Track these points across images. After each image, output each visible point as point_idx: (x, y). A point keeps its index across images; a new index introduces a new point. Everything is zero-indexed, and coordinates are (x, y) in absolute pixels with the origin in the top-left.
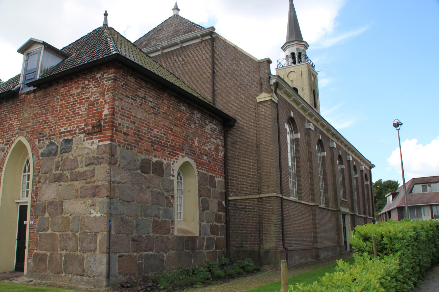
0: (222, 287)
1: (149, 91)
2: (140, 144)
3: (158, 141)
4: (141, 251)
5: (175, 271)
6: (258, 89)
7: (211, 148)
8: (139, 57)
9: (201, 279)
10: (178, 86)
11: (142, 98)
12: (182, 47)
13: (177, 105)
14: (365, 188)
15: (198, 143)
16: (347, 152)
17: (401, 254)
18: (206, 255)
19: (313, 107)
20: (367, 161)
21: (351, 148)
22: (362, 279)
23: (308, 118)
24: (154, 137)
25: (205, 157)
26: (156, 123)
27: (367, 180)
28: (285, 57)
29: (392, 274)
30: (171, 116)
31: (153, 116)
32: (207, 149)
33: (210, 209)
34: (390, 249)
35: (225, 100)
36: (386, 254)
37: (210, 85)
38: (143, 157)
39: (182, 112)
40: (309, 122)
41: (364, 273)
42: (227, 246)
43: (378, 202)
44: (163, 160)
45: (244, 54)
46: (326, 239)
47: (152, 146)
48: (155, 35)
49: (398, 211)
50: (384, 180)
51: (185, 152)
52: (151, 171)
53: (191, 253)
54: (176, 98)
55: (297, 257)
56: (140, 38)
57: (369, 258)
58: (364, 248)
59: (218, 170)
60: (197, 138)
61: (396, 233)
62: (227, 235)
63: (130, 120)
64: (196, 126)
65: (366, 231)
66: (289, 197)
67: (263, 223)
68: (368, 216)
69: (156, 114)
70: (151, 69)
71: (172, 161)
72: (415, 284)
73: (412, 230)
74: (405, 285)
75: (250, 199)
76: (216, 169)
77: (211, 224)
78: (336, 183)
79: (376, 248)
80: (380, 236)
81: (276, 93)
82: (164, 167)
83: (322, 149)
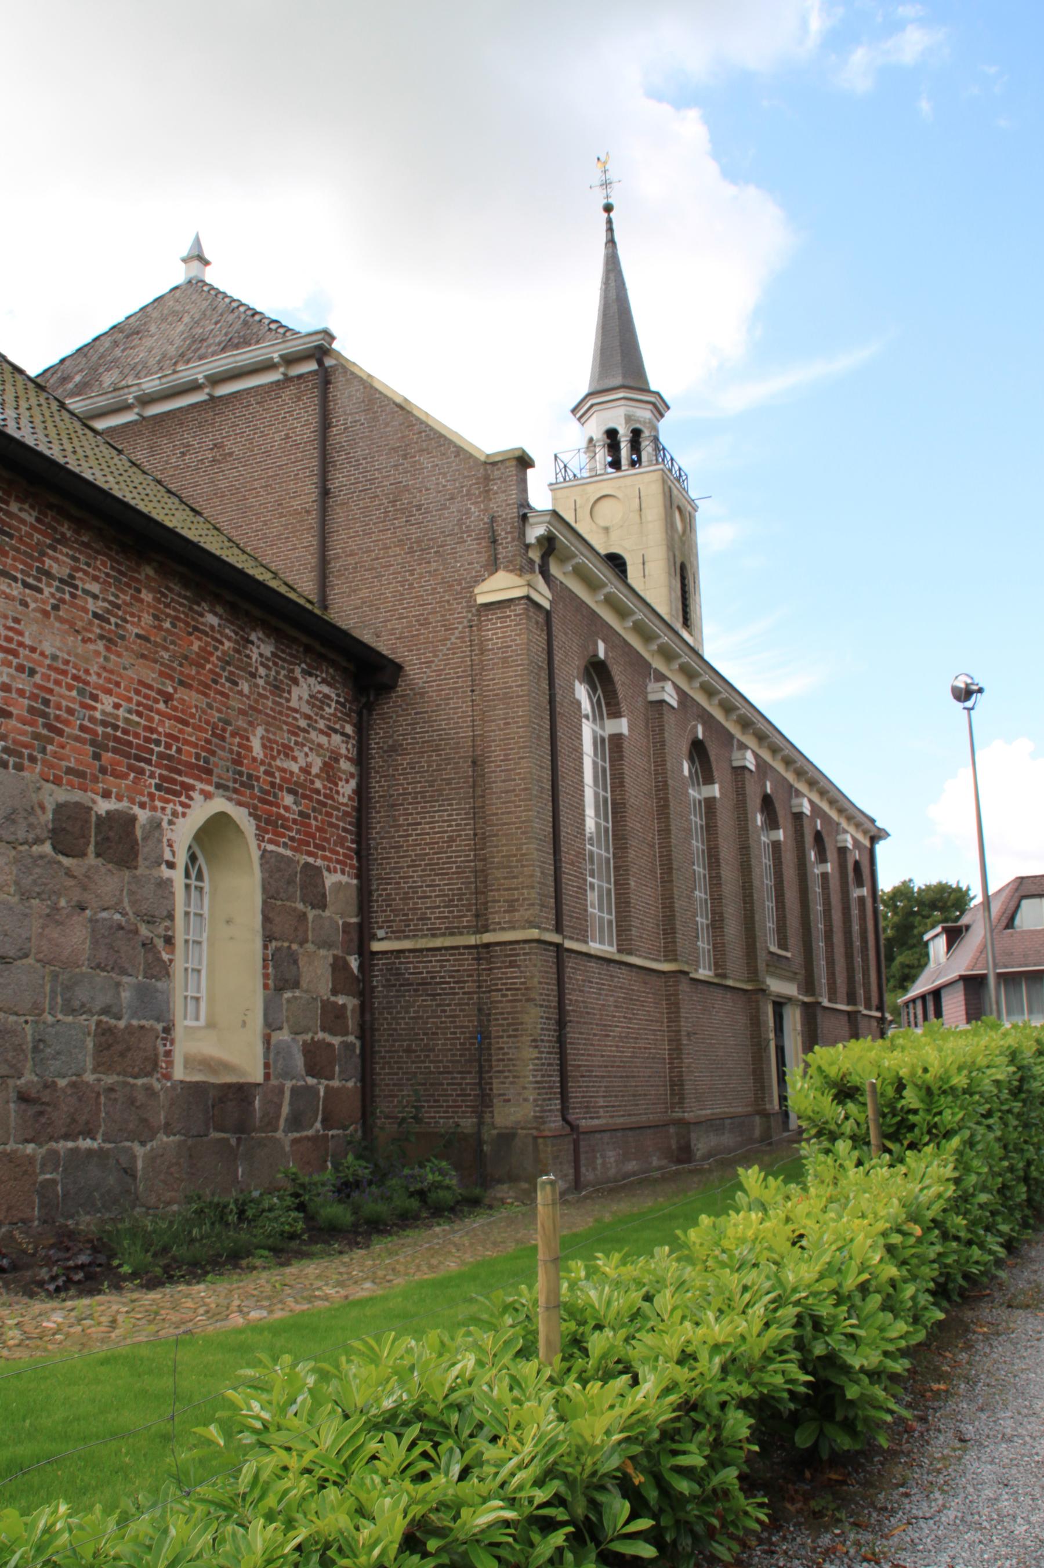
0: (344, 1264)
1: (89, 556)
2: (49, 747)
3: (117, 739)
4: (51, 1138)
5: (175, 1207)
6: (483, 558)
7: (309, 765)
8: (52, 432)
9: (269, 1236)
10: (195, 539)
11: (61, 581)
12: (212, 398)
13: (191, 609)
14: (855, 912)
15: (264, 746)
16: (791, 786)
17: (964, 1143)
18: (287, 1149)
19: (678, 626)
20: (861, 818)
21: (806, 773)
22: (821, 1238)
23: (658, 664)
24: (104, 724)
25: (288, 800)
26: (111, 672)
27: (860, 884)
28: (583, 444)
29: (930, 1214)
30: (167, 649)
31: (100, 646)
32: (295, 768)
33: (304, 984)
34: (925, 1130)
35: (364, 593)
36: (912, 1146)
37: (311, 540)
38: (63, 795)
39: (206, 634)
40: (661, 677)
41: (832, 1215)
42: (364, 1115)
43: (899, 959)
44: (136, 810)
45: (436, 432)
46: (715, 1090)
47: (97, 756)
48: (118, 352)
49: (966, 989)
50: (919, 883)
51: (215, 779)
52: (91, 848)
53: (233, 1142)
54: (186, 584)
55: (612, 1156)
56: (63, 361)
57: (855, 1161)
58: (839, 1126)
59: (335, 844)
60: (260, 731)
61: (946, 1071)
62: (363, 1080)
63: (15, 661)
64: (257, 686)
65: (847, 1066)
66: (586, 942)
67: (493, 1034)
68: (861, 1008)
69: (110, 642)
70: (99, 474)
71: (168, 811)
72: (1010, 1245)
73: (1004, 1060)
74: (975, 1247)
75: (446, 948)
76: (327, 840)
77: (308, 1037)
78: (751, 895)
79: (880, 1126)
80: (892, 1084)
81: (545, 573)
82: (139, 833)
83: (706, 775)
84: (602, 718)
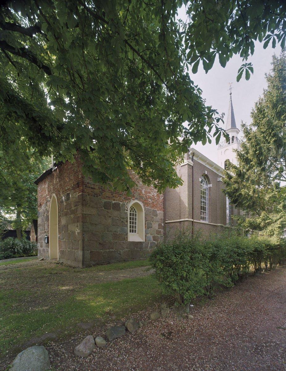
25: (150, 200)
32: (151, 195)
38: (106, 200)
44: (120, 202)
60: (144, 190)
84: (207, 184)
